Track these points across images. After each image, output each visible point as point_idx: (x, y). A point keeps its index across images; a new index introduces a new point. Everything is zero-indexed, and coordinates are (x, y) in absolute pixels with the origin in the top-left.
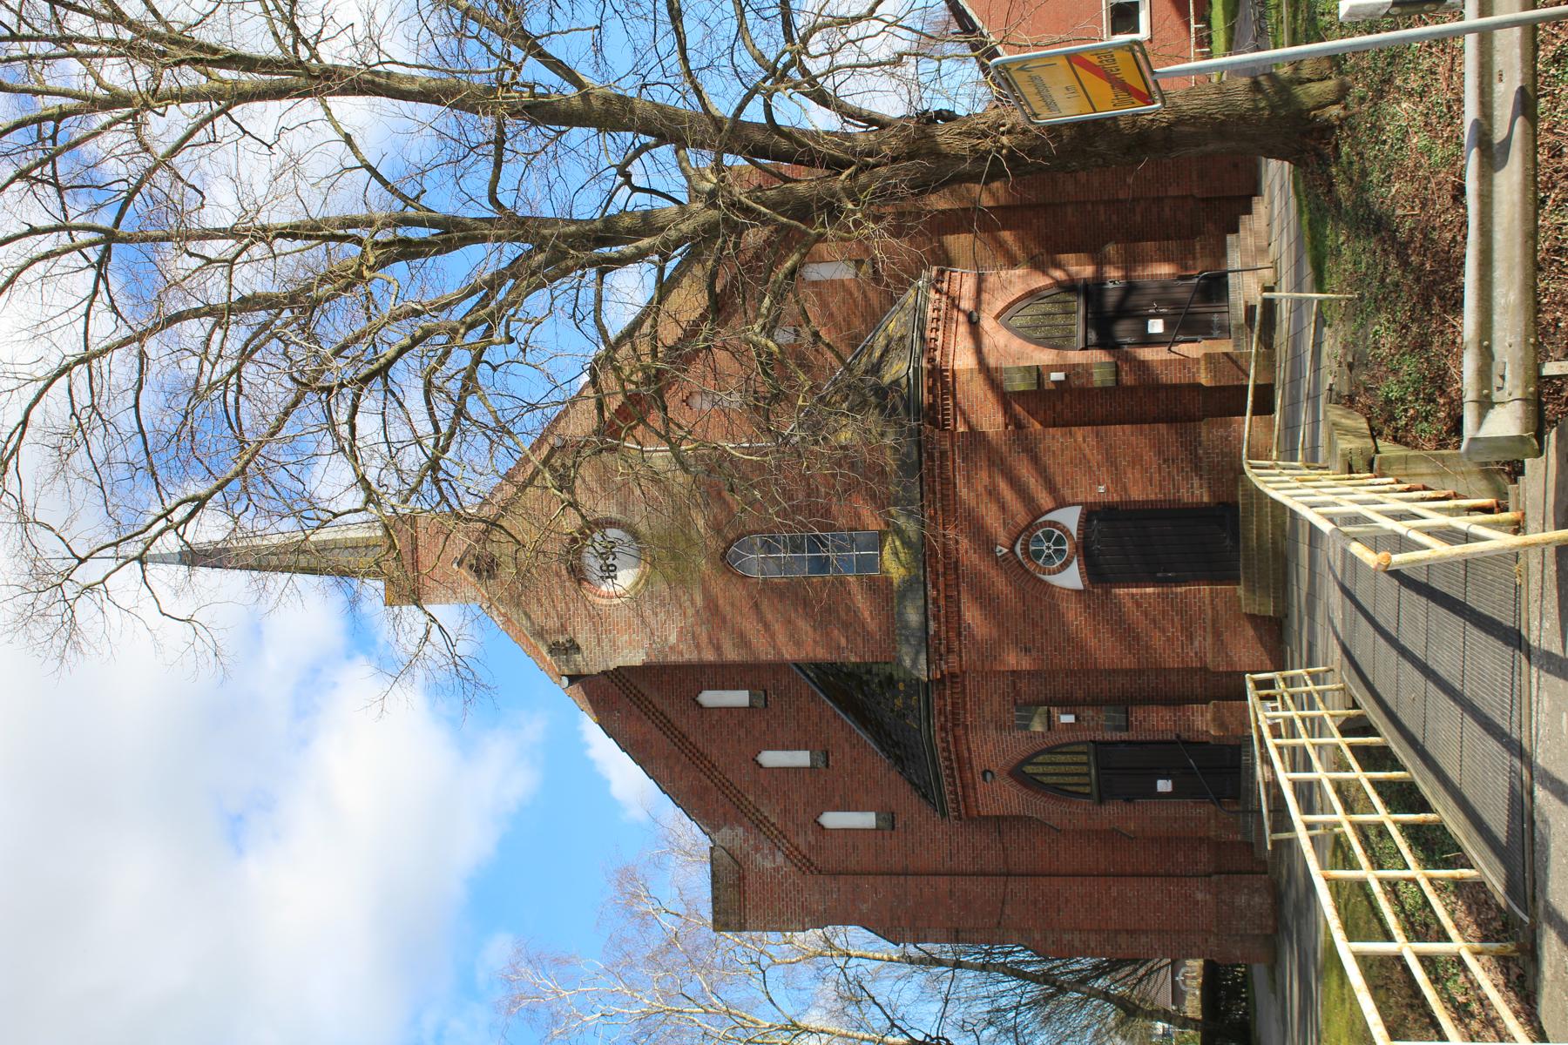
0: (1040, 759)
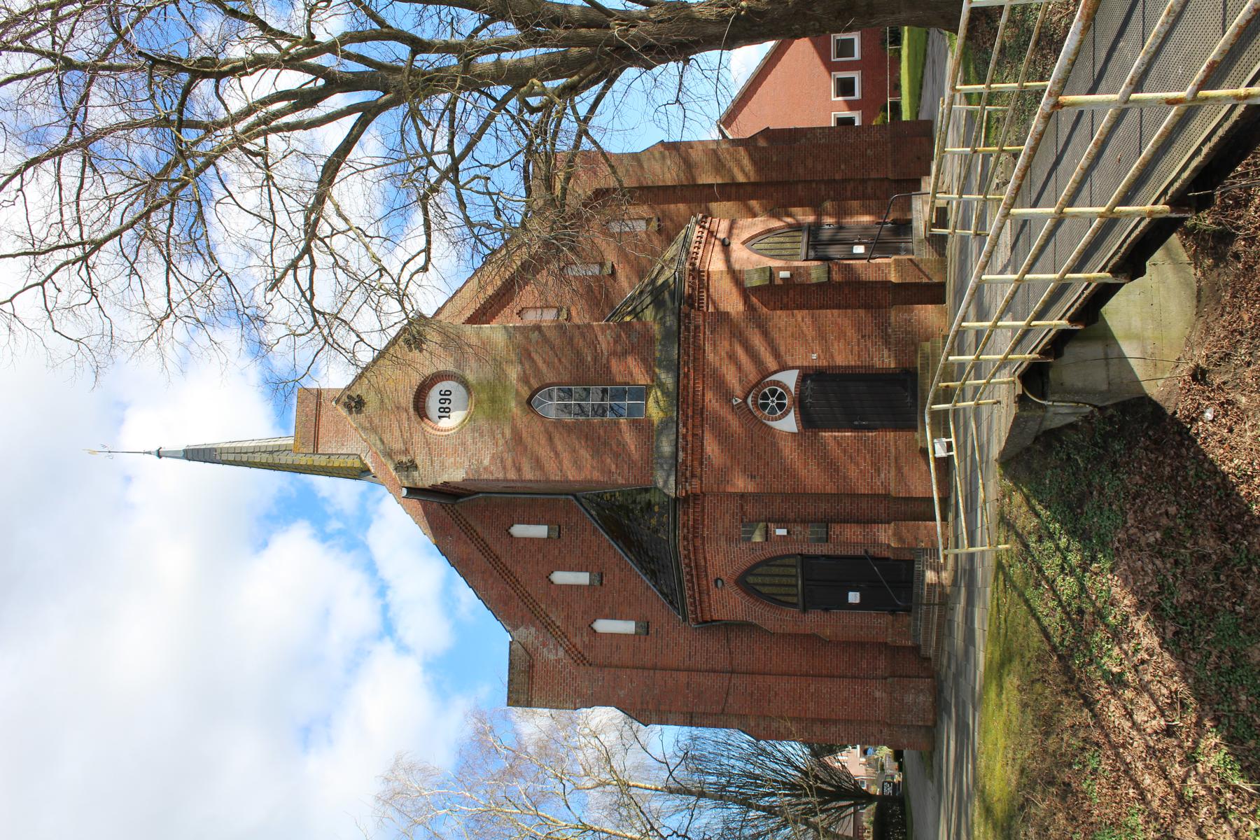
0: (759, 570)
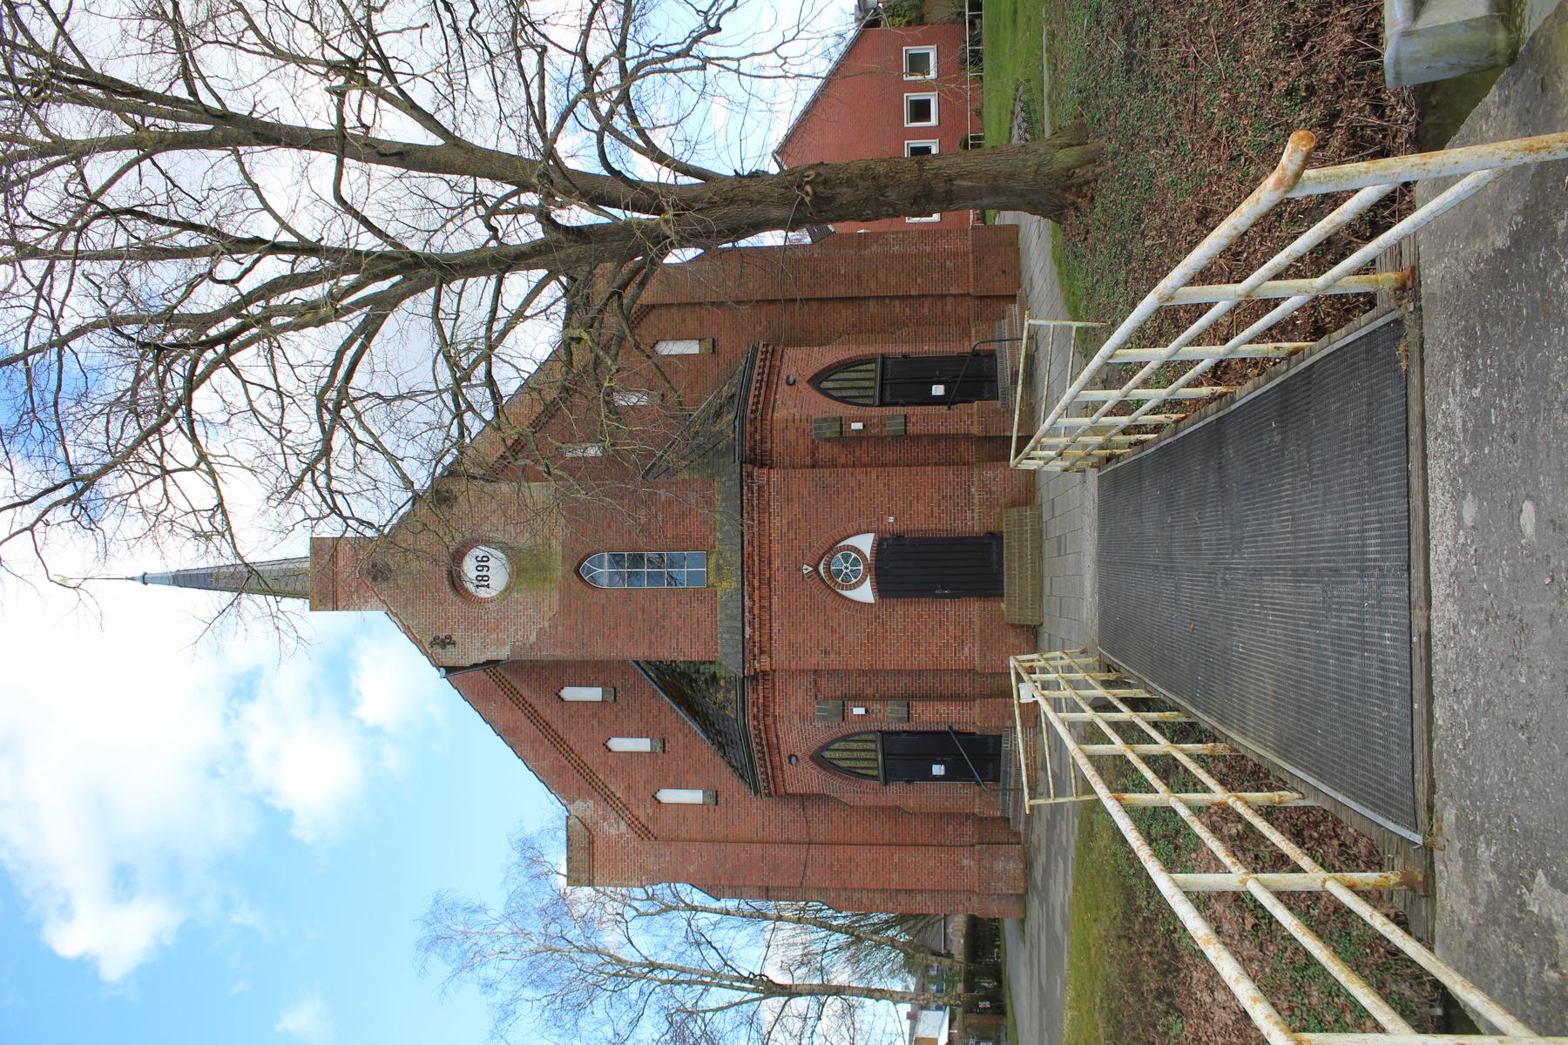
0: (836, 746)
